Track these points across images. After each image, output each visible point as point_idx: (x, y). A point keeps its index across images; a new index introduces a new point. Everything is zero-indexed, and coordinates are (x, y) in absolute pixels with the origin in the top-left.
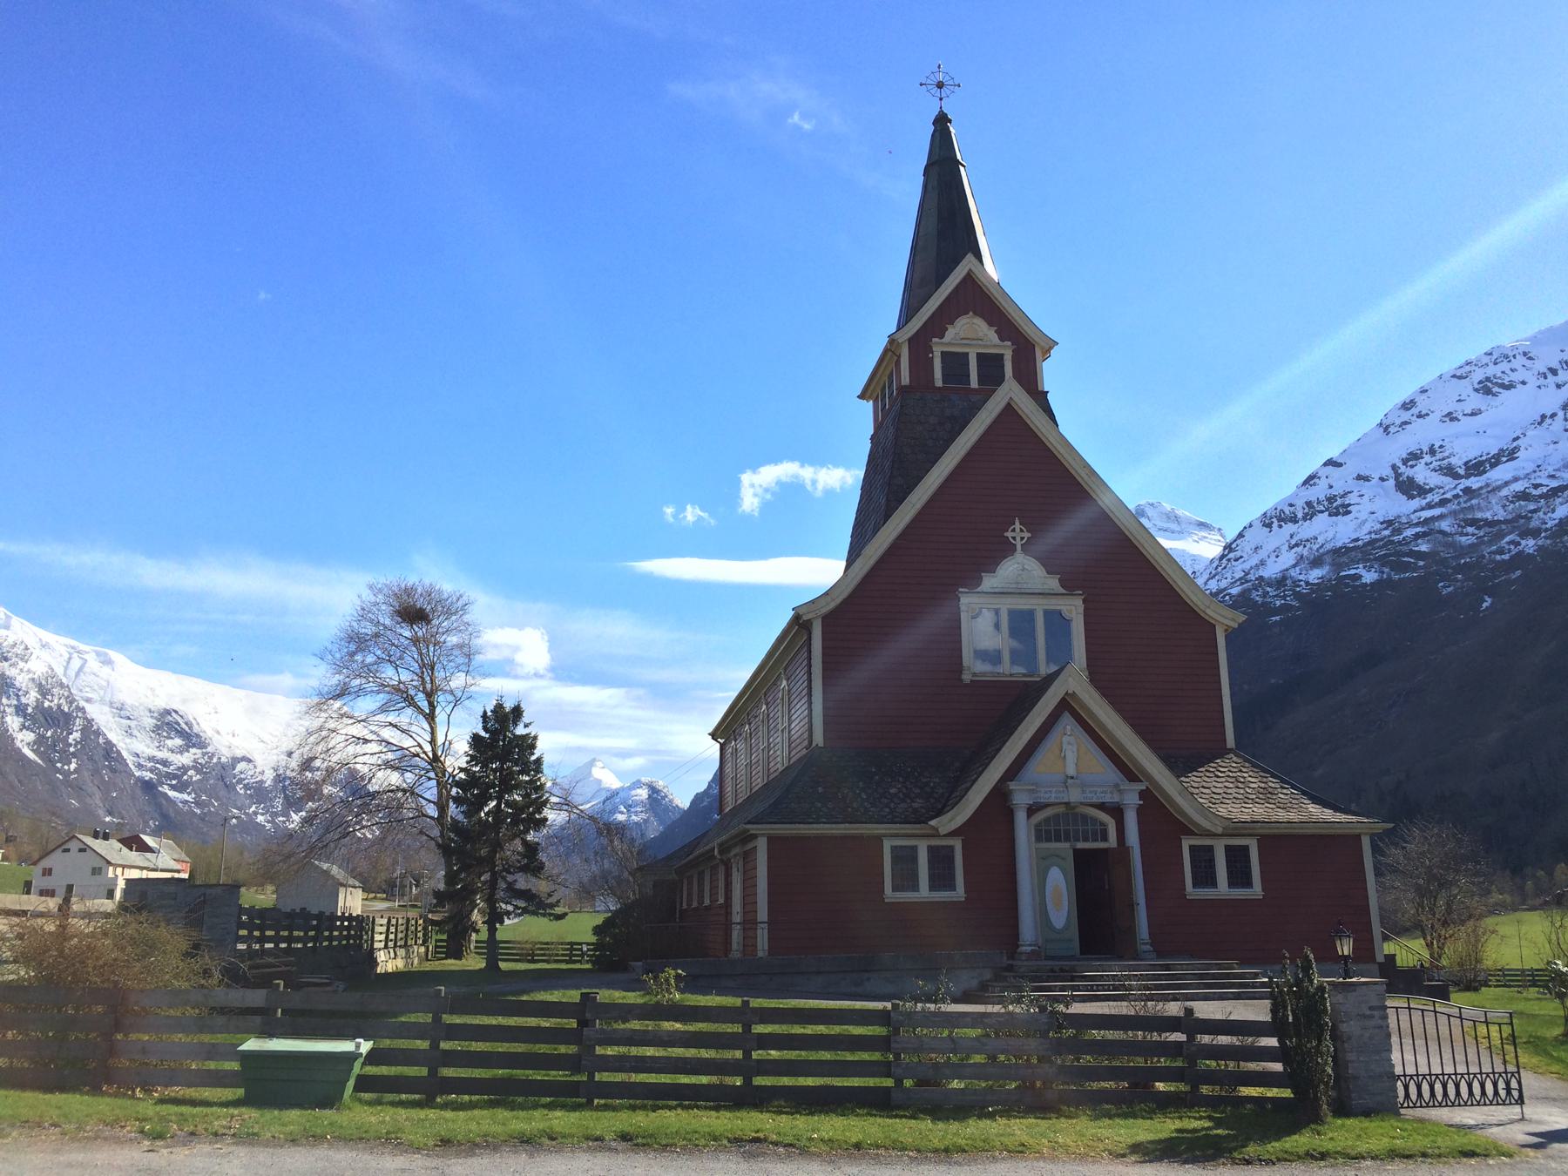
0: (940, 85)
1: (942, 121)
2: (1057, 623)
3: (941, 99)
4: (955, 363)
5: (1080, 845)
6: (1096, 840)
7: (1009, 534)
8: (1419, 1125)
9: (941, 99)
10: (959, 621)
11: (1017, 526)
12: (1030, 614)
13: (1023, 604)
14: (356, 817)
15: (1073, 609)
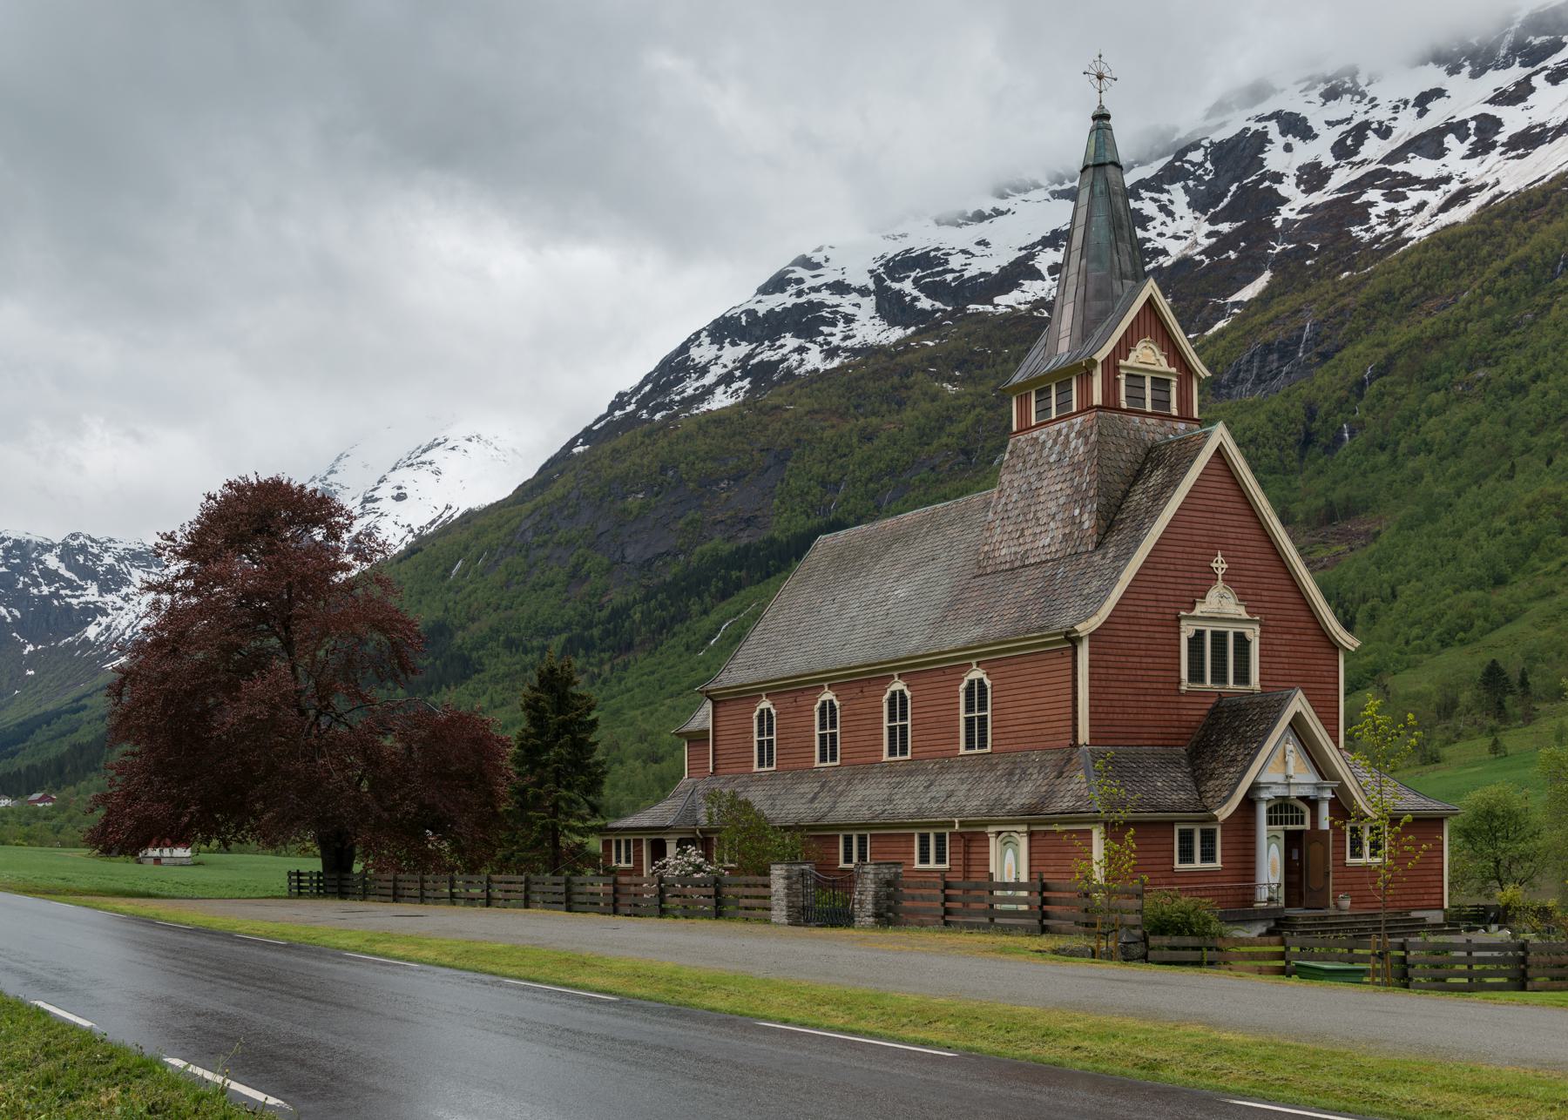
0: (1100, 77)
1: (1101, 117)
2: (1242, 642)
3: (1101, 92)
4: (1135, 379)
5: (1290, 827)
6: (1297, 823)
7: (1225, 566)
8: (1336, 1050)
9: (1101, 92)
10: (847, 528)
11: (1220, 558)
12: (1224, 635)
13: (1220, 627)
14: (271, 580)
15: (1253, 634)
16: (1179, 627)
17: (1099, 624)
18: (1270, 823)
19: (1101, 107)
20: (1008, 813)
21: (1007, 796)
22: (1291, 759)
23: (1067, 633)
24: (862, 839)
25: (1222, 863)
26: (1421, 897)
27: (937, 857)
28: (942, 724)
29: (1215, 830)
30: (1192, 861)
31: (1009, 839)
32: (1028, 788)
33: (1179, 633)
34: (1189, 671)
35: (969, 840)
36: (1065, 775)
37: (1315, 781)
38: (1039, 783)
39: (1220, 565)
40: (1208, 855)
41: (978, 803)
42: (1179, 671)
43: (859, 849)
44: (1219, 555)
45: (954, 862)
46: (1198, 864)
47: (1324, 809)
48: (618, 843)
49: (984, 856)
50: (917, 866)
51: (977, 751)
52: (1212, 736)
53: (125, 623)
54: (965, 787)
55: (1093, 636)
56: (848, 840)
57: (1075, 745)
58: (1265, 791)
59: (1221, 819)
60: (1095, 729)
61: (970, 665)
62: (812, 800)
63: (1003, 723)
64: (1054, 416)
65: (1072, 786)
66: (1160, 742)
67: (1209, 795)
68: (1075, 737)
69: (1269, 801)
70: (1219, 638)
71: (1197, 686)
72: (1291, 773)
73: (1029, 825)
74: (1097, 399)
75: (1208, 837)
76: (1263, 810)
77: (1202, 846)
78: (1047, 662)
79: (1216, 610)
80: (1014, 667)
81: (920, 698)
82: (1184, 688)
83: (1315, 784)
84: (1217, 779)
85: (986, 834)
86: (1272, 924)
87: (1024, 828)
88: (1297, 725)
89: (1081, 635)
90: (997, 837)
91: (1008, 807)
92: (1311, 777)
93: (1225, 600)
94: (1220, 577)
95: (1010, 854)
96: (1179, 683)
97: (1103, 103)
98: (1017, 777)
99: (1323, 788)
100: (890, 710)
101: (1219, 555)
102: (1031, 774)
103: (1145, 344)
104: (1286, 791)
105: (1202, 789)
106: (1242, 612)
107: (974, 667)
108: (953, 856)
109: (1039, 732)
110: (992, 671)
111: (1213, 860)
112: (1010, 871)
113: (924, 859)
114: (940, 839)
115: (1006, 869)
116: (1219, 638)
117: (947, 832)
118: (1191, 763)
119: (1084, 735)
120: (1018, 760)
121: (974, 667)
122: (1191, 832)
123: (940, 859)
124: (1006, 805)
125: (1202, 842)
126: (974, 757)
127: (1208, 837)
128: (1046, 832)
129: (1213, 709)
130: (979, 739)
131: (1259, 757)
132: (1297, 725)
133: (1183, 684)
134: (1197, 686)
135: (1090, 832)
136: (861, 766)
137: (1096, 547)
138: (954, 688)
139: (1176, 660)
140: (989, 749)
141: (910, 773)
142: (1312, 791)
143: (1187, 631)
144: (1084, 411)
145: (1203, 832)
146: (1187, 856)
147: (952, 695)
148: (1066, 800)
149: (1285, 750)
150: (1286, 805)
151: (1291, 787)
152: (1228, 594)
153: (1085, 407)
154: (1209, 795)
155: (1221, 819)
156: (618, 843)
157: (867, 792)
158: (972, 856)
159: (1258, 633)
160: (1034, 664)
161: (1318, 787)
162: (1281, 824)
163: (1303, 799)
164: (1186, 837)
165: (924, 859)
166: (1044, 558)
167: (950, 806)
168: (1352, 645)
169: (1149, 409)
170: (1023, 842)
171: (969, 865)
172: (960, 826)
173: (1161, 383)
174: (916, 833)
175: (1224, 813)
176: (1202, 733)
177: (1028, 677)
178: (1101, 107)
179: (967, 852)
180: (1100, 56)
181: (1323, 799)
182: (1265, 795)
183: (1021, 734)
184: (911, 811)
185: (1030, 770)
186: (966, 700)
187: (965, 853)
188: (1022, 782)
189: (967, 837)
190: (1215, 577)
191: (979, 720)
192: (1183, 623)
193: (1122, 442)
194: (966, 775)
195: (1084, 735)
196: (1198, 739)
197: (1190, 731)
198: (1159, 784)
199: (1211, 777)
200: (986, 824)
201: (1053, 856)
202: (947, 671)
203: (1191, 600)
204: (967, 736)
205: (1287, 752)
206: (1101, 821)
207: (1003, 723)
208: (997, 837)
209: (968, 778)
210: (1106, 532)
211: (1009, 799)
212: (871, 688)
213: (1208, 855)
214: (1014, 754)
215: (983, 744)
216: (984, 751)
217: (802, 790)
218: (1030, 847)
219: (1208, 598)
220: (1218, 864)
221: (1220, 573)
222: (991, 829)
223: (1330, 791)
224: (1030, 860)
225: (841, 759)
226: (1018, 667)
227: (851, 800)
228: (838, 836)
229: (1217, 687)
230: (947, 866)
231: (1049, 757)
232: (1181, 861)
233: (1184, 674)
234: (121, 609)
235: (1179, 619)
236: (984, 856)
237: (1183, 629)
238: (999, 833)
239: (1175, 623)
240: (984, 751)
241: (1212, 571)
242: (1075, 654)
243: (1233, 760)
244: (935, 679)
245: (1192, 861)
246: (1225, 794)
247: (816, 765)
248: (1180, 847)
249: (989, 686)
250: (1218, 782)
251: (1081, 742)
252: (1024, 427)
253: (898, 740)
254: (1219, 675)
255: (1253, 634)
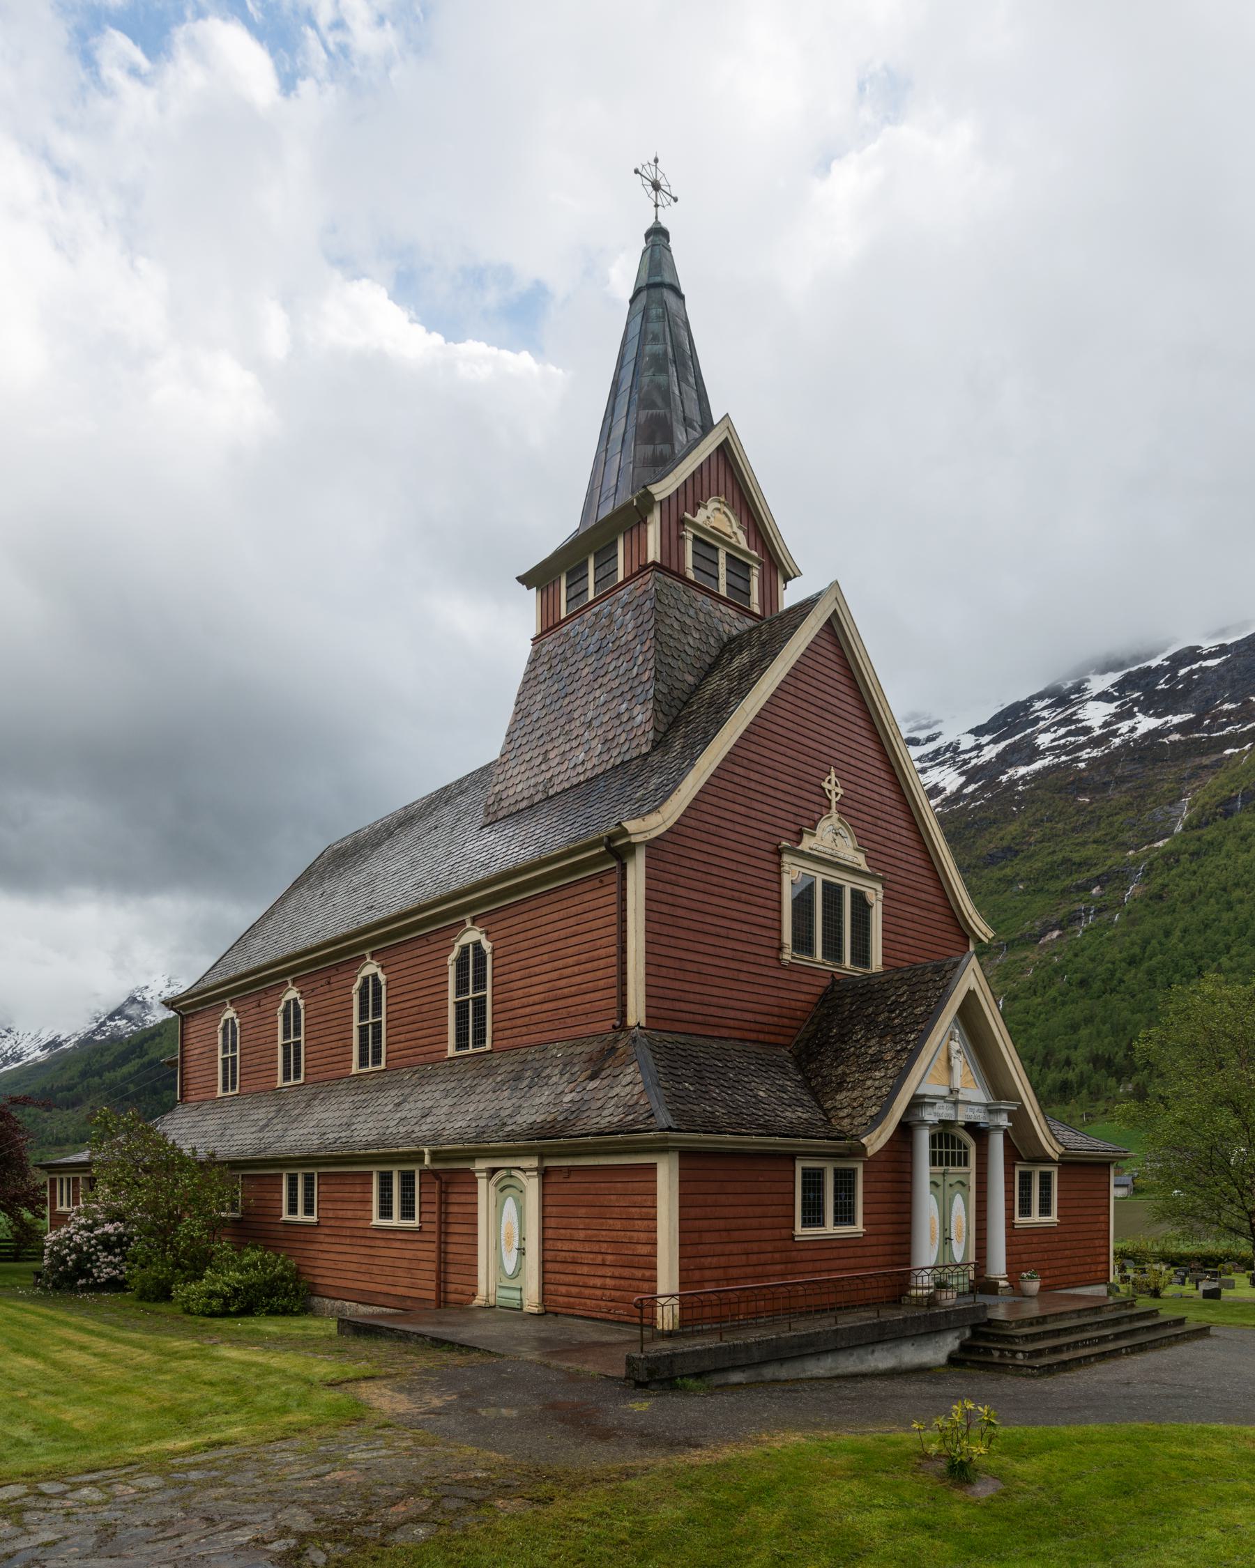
1: (657, 235)
2: (861, 905)
3: (657, 206)
13: (836, 877)
15: (875, 895)
16: (779, 865)
17: (662, 829)
18: (933, 1163)
19: (657, 222)
20: (509, 1137)
21: (508, 1112)
22: (958, 1063)
23: (612, 838)
24: (309, 1179)
25: (865, 1225)
26: (1087, 1268)
27: (403, 1208)
28: (425, 1016)
29: (854, 1171)
30: (820, 1222)
31: (507, 1182)
32: (543, 1096)
33: (779, 874)
34: (794, 934)
35: (448, 1184)
36: (603, 1074)
37: (984, 1101)
38: (560, 1089)
39: (833, 787)
40: (844, 1215)
41: (464, 1124)
42: (780, 931)
43: (403, 1196)
44: (833, 774)
45: (426, 1217)
46: (830, 1228)
47: (997, 1144)
48: (62, 1180)
49: (469, 1209)
50: (377, 1221)
51: (471, 1050)
52: (830, 1030)
53: (7, 1046)
54: (450, 1101)
55: (650, 845)
56: (386, 1180)
57: (623, 1027)
58: (929, 1110)
59: (871, 1151)
60: (654, 1002)
61: (463, 923)
62: (262, 1130)
63: (509, 1005)
64: (591, 597)
65: (617, 1090)
66: (753, 1036)
67: (841, 1114)
68: (623, 1014)
69: (933, 1126)
70: (833, 892)
71: (803, 960)
72: (957, 1084)
73: (542, 1157)
74: (653, 552)
75: (845, 1182)
76: (924, 1138)
77: (836, 1197)
78: (577, 900)
79: (830, 851)
80: (525, 917)
81: (398, 983)
82: (787, 956)
83: (987, 1105)
84: (853, 1089)
85: (473, 1173)
86: (968, 1333)
87: (533, 1162)
88: (969, 1014)
89: (634, 839)
90: (489, 1178)
91: (509, 1128)
92: (975, 1092)
93: (838, 839)
94: (834, 804)
95: (510, 1206)
96: (780, 949)
97: (659, 220)
98: (526, 1082)
99: (999, 1111)
100: (361, 1004)
101: (833, 774)
102: (549, 1077)
103: (718, 505)
104: (951, 1112)
105: (828, 1105)
106: (860, 860)
107: (469, 925)
108: (426, 1208)
109: (564, 1013)
110: (493, 928)
111: (852, 1221)
112: (509, 1236)
113: (386, 1212)
114: (407, 1179)
115: (503, 1232)
116: (833, 892)
117: (416, 1168)
118: (801, 1069)
119: (636, 1012)
120: (530, 1058)
121: (469, 925)
122: (820, 1173)
123: (407, 1213)
124: (505, 1124)
125: (836, 1190)
126: (468, 1059)
127: (845, 1182)
128: (570, 1170)
129: (825, 994)
130: (474, 1032)
131: (923, 1053)
132: (969, 1014)
133: (786, 950)
134: (803, 960)
135: (652, 1168)
136: (326, 1083)
137: (654, 748)
138: (441, 962)
139: (549, 1255)
140: (488, 1046)
141: (381, 1088)
142: (982, 1115)
143: (793, 873)
144: (638, 573)
145: (838, 1173)
146: (814, 1215)
147: (439, 971)
148: (606, 1113)
149: (948, 1049)
150: (947, 1135)
151: (960, 1107)
152: (843, 832)
153: (635, 569)
154: (841, 1114)
155: (871, 1151)
156: (62, 1180)
157: (325, 1115)
158: (453, 1209)
159: (880, 896)
160: (558, 906)
161: (991, 1111)
162: (941, 1165)
163: (971, 1127)
164: (813, 1181)
165: (386, 1212)
166: (575, 781)
167: (424, 1129)
168: (985, 935)
169: (723, 591)
170: (532, 1186)
171: (447, 1223)
172: (433, 1160)
173: (738, 566)
174: (375, 1170)
175: (876, 1141)
176: (812, 1028)
177: (549, 928)
178: (657, 222)
179: (444, 1203)
180: (656, 161)
181: (998, 1127)
182: (930, 1115)
183: (535, 1018)
184: (370, 1138)
185: (548, 1071)
186: (458, 977)
187: (441, 1203)
188: (534, 1090)
189: (444, 1177)
190: (825, 802)
191: (475, 1004)
192: (786, 858)
193: (688, 621)
194: (453, 1084)
195: (636, 1012)
196: (807, 1036)
197: (794, 1023)
198: (761, 1094)
199: (840, 1087)
200: (472, 1156)
201: (582, 1211)
202: (433, 938)
203: (795, 828)
204: (458, 1030)
205: (953, 1054)
206: (673, 1149)
207: (509, 1005)
208: (489, 1178)
209: (454, 1088)
210: (668, 730)
211: (511, 1116)
212: (339, 977)
213: (844, 1215)
214: (523, 1051)
215: (480, 1039)
216: (481, 1049)
217: (256, 1117)
218: (543, 1195)
219: (819, 831)
220: (859, 1227)
221: (834, 799)
222: (480, 1165)
223: (1005, 1116)
224: (544, 1217)
225: (306, 1075)
226: (531, 914)
227: (305, 1127)
228: (280, 1176)
229: (830, 966)
230: (415, 1223)
231: (579, 1050)
232: (805, 1224)
233: (787, 938)
234: (5, 1037)
235: (779, 852)
236: (469, 1209)
237: (786, 868)
238: (494, 1171)
239: (775, 858)
240: (481, 1049)
241: (823, 794)
242: (624, 877)
243: (876, 1061)
244: (418, 952)
245: (820, 1222)
246: (875, 1110)
247: (279, 1085)
248: (804, 1198)
249: (488, 951)
250: (856, 1094)
251: (631, 1021)
252: (551, 624)
253: (370, 1049)
254: (832, 949)
255: (875, 895)
